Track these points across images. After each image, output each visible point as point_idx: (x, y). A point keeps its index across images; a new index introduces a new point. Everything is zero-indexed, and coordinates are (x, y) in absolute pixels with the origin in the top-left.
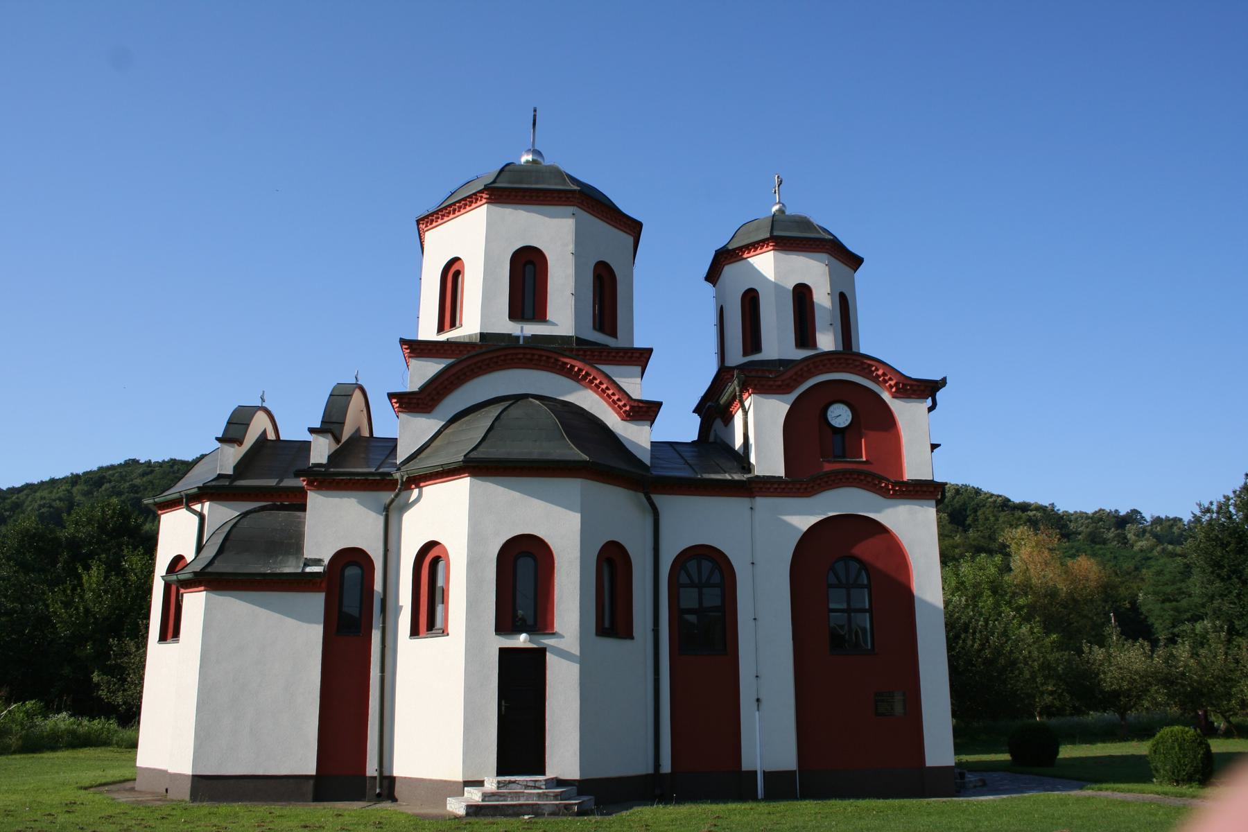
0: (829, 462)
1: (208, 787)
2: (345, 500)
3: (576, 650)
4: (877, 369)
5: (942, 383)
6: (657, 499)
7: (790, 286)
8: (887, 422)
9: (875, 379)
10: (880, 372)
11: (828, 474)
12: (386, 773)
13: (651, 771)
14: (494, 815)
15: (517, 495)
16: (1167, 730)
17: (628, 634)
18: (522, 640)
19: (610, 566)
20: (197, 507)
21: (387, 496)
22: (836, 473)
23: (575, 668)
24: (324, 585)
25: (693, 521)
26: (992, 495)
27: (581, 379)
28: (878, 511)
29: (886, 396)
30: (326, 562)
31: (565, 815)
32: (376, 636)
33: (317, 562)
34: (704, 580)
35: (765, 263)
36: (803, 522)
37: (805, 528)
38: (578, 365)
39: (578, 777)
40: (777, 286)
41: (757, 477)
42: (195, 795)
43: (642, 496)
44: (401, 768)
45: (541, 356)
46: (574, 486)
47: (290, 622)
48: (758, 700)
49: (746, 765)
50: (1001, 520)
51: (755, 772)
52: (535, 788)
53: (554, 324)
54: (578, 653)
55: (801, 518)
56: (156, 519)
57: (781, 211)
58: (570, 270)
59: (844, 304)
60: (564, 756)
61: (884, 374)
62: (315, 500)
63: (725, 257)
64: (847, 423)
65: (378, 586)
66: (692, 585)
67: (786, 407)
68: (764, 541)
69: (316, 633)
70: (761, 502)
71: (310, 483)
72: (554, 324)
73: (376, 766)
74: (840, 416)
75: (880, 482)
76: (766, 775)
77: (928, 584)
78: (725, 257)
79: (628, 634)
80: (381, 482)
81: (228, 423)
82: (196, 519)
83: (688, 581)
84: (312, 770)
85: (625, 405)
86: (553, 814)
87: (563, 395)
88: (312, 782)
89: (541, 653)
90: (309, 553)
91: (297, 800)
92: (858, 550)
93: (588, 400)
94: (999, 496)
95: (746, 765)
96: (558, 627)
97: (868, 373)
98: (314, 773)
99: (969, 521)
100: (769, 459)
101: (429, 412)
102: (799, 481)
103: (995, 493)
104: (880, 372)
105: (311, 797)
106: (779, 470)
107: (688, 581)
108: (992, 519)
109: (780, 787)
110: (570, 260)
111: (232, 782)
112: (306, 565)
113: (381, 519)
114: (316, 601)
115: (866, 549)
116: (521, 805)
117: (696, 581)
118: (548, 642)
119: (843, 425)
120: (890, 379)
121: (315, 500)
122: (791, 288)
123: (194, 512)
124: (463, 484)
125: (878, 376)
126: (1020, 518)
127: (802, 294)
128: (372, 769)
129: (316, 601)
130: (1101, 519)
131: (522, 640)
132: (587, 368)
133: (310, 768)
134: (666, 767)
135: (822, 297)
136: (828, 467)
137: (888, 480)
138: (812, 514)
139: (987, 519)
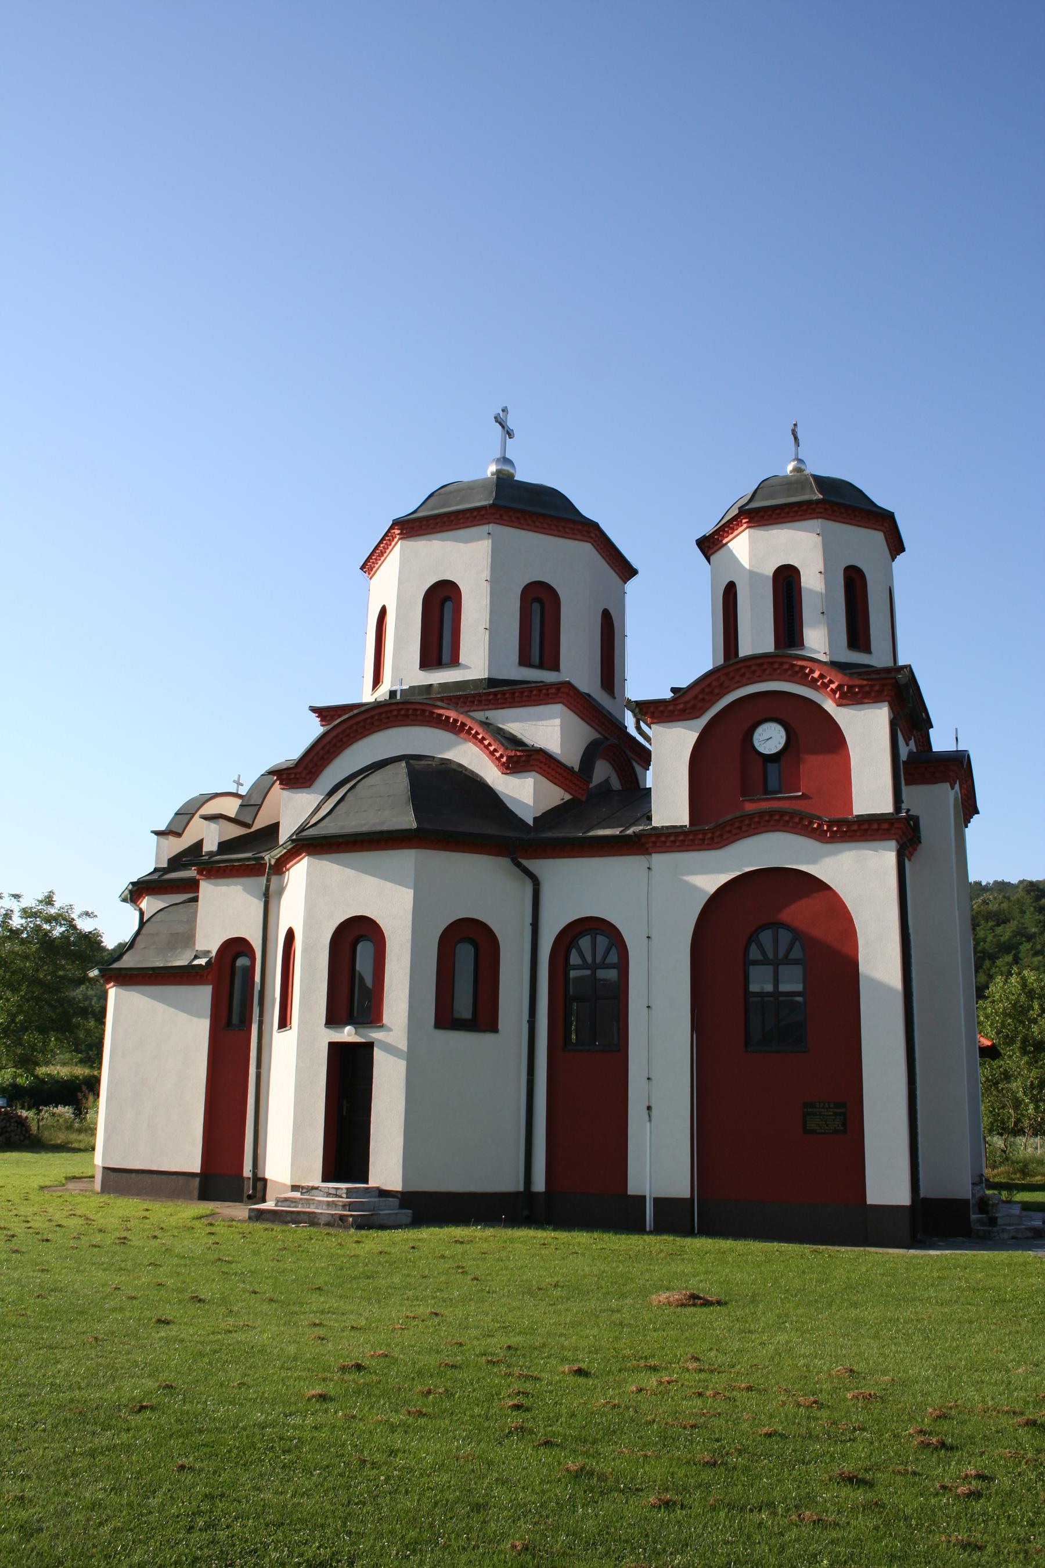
0: (751, 801)
2: (232, 887)
3: (403, 1045)
4: (812, 671)
6: (535, 865)
7: (770, 571)
8: (834, 740)
9: (812, 684)
10: (816, 675)
11: (751, 816)
12: (260, 1175)
14: (273, 1222)
15: (350, 872)
17: (492, 1026)
18: (348, 1034)
19: (464, 953)
22: (761, 814)
23: (402, 1065)
24: (210, 977)
25: (581, 886)
27: (457, 729)
28: (813, 861)
29: (829, 706)
30: (214, 954)
31: (339, 1226)
33: (207, 953)
34: (598, 961)
35: (742, 545)
36: (710, 883)
37: (712, 890)
38: (452, 714)
39: (399, 1188)
40: (752, 574)
41: (655, 828)
42: (105, 1188)
43: (505, 862)
45: (415, 710)
46: (407, 858)
47: (183, 1016)
48: (649, 1108)
49: (632, 1189)
51: (645, 1197)
52: (336, 1196)
54: (405, 1048)
55: (708, 875)
56: (979, 888)
57: (797, 470)
58: (485, 601)
59: (854, 583)
60: (387, 1169)
61: (822, 676)
62: (207, 889)
63: (710, 545)
64: (780, 747)
65: (257, 978)
66: (765, 962)
67: (694, 736)
68: (656, 907)
69: (201, 1028)
70: (659, 860)
71: (200, 872)
73: (251, 1168)
74: (770, 738)
75: (811, 823)
76: (658, 1202)
77: (880, 960)
78: (710, 545)
79: (492, 1026)
80: (254, 869)
81: (176, 814)
82: (137, 913)
83: (760, 957)
84: (196, 1168)
85: (502, 756)
86: (328, 1224)
87: (441, 752)
89: (369, 1046)
90: (200, 945)
91: (185, 1198)
92: (786, 915)
93: (472, 757)
95: (632, 1189)
96: (386, 1020)
98: (199, 1171)
100: (670, 802)
101: (309, 787)
102: (706, 830)
104: (816, 675)
105: (196, 1194)
107: (760, 957)
109: (673, 1218)
110: (486, 588)
111: (133, 1175)
112: (196, 957)
113: (258, 906)
115: (799, 913)
116: (299, 1212)
117: (589, 960)
118: (376, 1035)
119: (774, 751)
120: (831, 682)
121: (207, 889)
122: (771, 574)
125: (815, 680)
127: (786, 579)
128: (247, 1171)
131: (348, 1034)
132: (461, 718)
133: (195, 1166)
134: (539, 1184)
135: (812, 580)
136: (750, 807)
137: (819, 818)
138: (733, 871)
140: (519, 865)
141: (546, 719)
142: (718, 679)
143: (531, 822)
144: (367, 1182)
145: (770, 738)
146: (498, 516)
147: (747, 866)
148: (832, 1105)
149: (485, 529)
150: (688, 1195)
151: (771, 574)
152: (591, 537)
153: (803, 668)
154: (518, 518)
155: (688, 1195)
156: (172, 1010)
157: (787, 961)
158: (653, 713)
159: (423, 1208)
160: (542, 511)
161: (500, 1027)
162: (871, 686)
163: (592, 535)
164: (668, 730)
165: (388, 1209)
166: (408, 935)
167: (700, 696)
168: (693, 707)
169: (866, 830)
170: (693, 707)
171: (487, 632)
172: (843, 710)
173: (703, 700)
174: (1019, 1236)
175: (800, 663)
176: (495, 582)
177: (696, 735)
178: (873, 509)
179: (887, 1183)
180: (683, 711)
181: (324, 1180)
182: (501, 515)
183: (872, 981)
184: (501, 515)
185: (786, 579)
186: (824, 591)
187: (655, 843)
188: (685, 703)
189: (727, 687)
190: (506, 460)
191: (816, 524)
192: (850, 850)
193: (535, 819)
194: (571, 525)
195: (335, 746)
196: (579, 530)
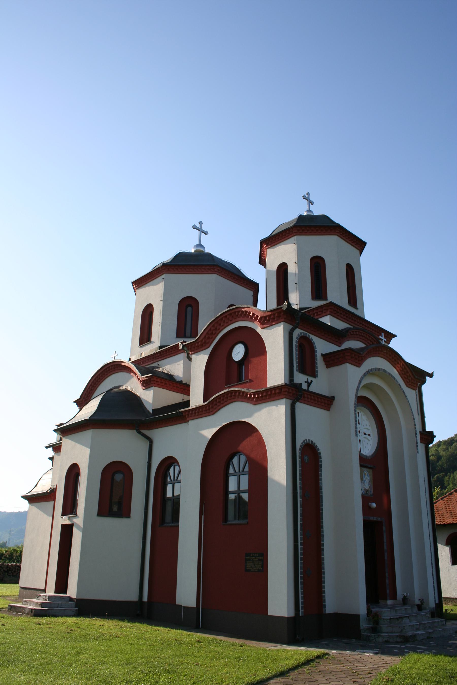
4: (250, 313)
6: (151, 433)
17: (128, 515)
23: (81, 534)
36: (209, 433)
39: (75, 597)
55: (207, 429)
79: (128, 515)
134: (145, 599)
138: (218, 426)
140: (139, 433)
141: (177, 362)
142: (213, 326)
143: (151, 411)
144: (66, 593)
145: (238, 352)
146: (167, 270)
147: (224, 422)
148: (257, 555)
149: (161, 277)
150: (194, 605)
151: (276, 270)
152: (216, 271)
153: (246, 312)
154: (185, 269)
155: (194, 605)
156: (43, 513)
157: (243, 472)
158: (191, 349)
159: (86, 608)
160: (187, 263)
161: (131, 515)
162: (274, 314)
163: (216, 270)
164: (198, 356)
165: (72, 607)
166: (87, 472)
167: (207, 336)
168: (205, 342)
169: (270, 395)
170: (205, 342)
171: (161, 324)
172: (265, 330)
173: (209, 338)
174: (391, 640)
175: (244, 310)
176: (165, 301)
177: (207, 356)
178: (334, 225)
179: (280, 601)
180: (202, 345)
181: (55, 593)
182: (169, 269)
183: (273, 481)
184: (169, 269)
185: (283, 269)
186: (297, 272)
187: (188, 415)
188: (201, 341)
189: (219, 329)
190: (200, 245)
191: (294, 239)
192: (265, 407)
193: (154, 410)
194: (208, 267)
195: (93, 386)
196: (204, 269)
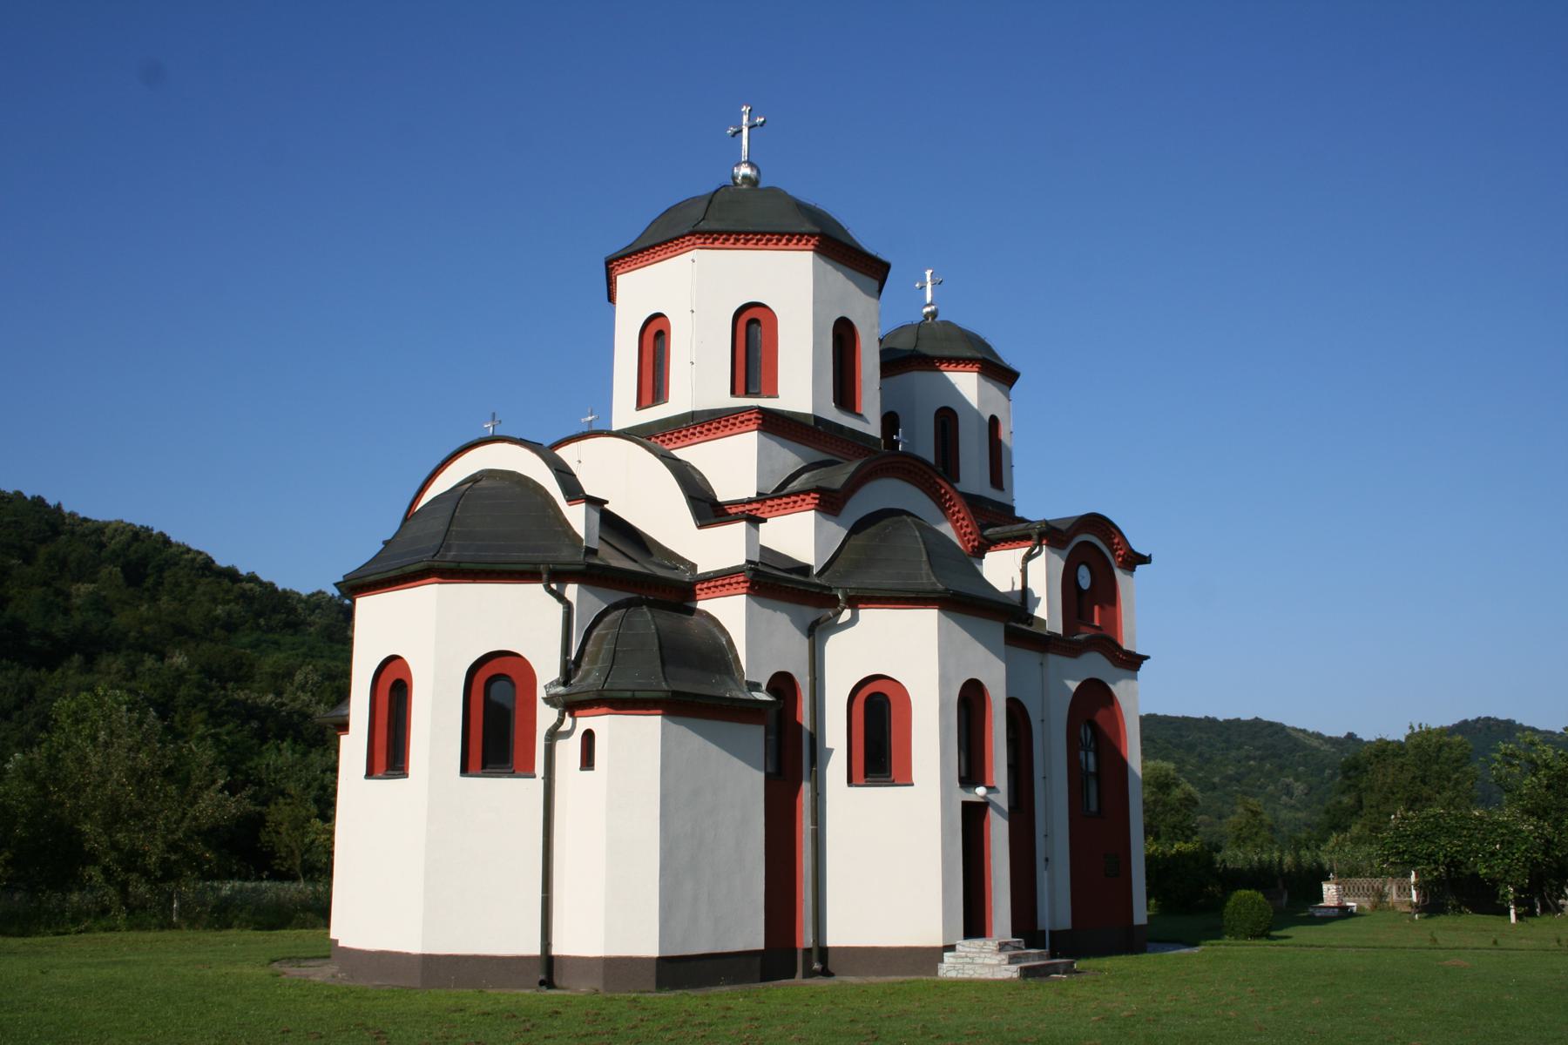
1: (675, 971)
3: (1005, 807)
5: (1145, 560)
13: (535, 950)
16: (1243, 893)
20: (572, 591)
21: (810, 613)
26: (189, 550)
32: (806, 787)
44: (834, 939)
49: (1040, 928)
50: (200, 589)
53: (860, 416)
57: (934, 314)
72: (860, 416)
88: (758, 959)
94: (200, 553)
95: (1040, 928)
97: (1110, 546)
99: (149, 582)
103: (194, 547)
106: (1056, 626)
108: (186, 585)
114: (755, 735)
123: (560, 597)
124: (929, 618)
126: (228, 592)
129: (755, 735)
130: (318, 606)
139: (177, 584)
